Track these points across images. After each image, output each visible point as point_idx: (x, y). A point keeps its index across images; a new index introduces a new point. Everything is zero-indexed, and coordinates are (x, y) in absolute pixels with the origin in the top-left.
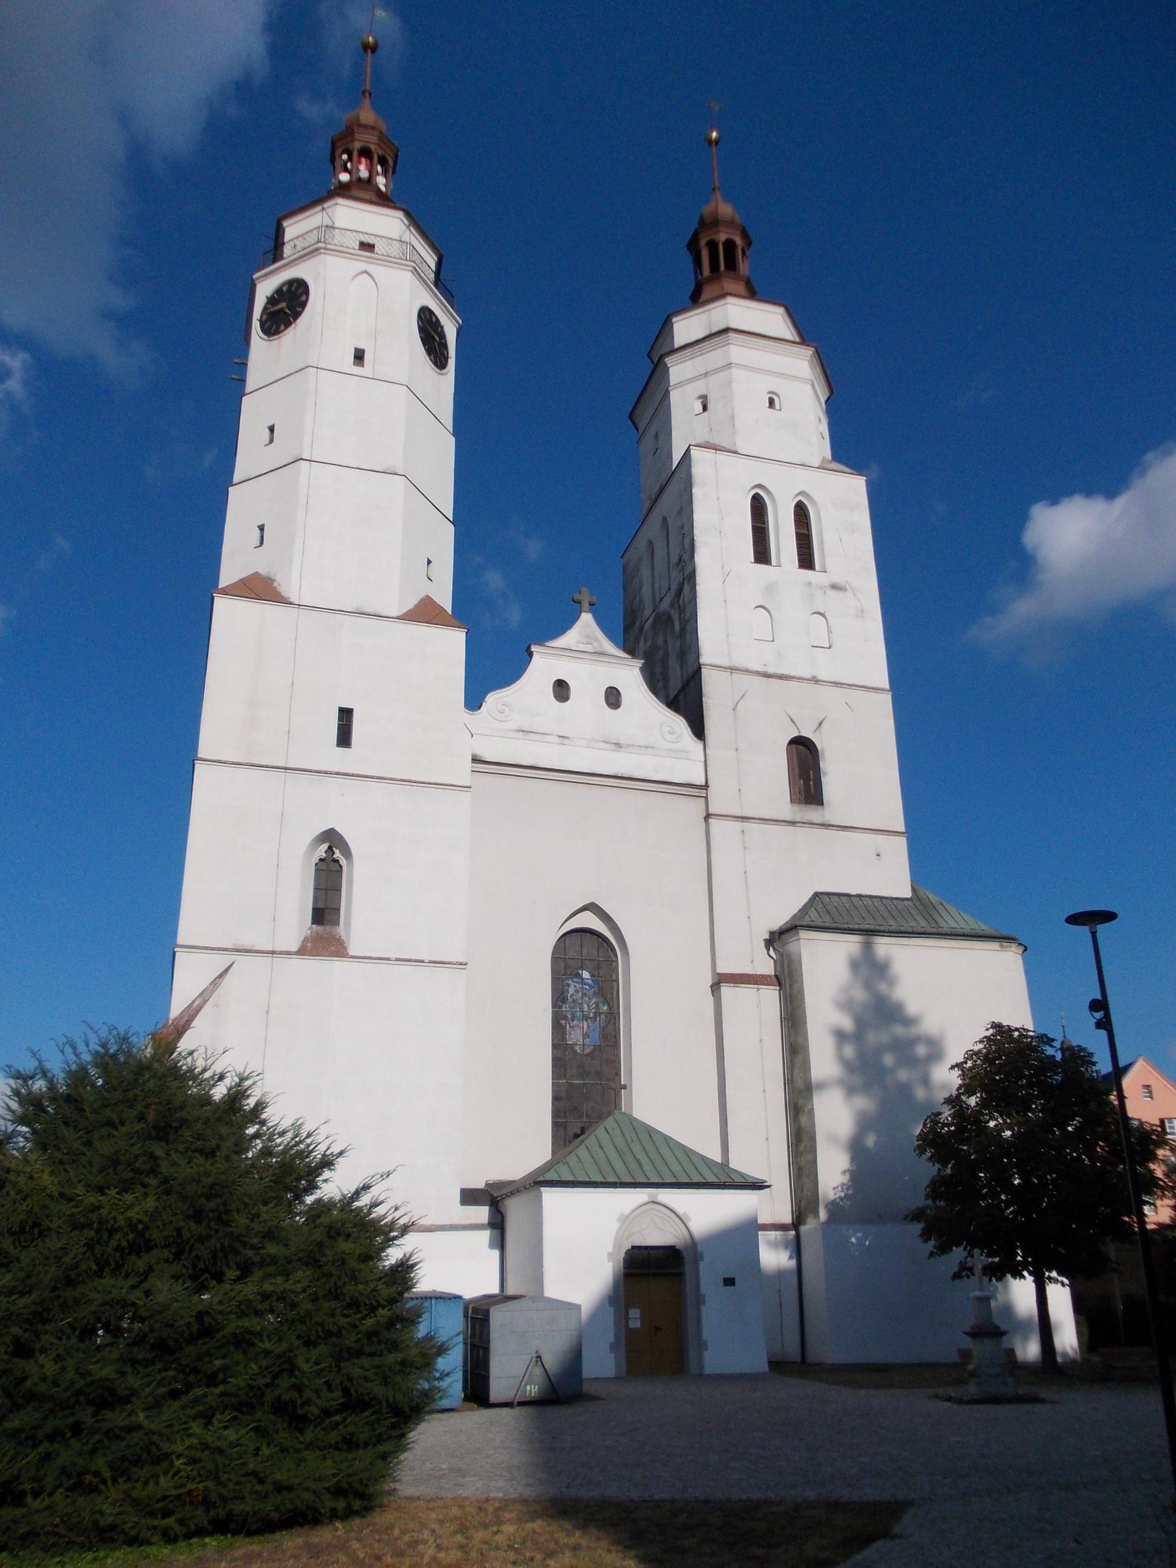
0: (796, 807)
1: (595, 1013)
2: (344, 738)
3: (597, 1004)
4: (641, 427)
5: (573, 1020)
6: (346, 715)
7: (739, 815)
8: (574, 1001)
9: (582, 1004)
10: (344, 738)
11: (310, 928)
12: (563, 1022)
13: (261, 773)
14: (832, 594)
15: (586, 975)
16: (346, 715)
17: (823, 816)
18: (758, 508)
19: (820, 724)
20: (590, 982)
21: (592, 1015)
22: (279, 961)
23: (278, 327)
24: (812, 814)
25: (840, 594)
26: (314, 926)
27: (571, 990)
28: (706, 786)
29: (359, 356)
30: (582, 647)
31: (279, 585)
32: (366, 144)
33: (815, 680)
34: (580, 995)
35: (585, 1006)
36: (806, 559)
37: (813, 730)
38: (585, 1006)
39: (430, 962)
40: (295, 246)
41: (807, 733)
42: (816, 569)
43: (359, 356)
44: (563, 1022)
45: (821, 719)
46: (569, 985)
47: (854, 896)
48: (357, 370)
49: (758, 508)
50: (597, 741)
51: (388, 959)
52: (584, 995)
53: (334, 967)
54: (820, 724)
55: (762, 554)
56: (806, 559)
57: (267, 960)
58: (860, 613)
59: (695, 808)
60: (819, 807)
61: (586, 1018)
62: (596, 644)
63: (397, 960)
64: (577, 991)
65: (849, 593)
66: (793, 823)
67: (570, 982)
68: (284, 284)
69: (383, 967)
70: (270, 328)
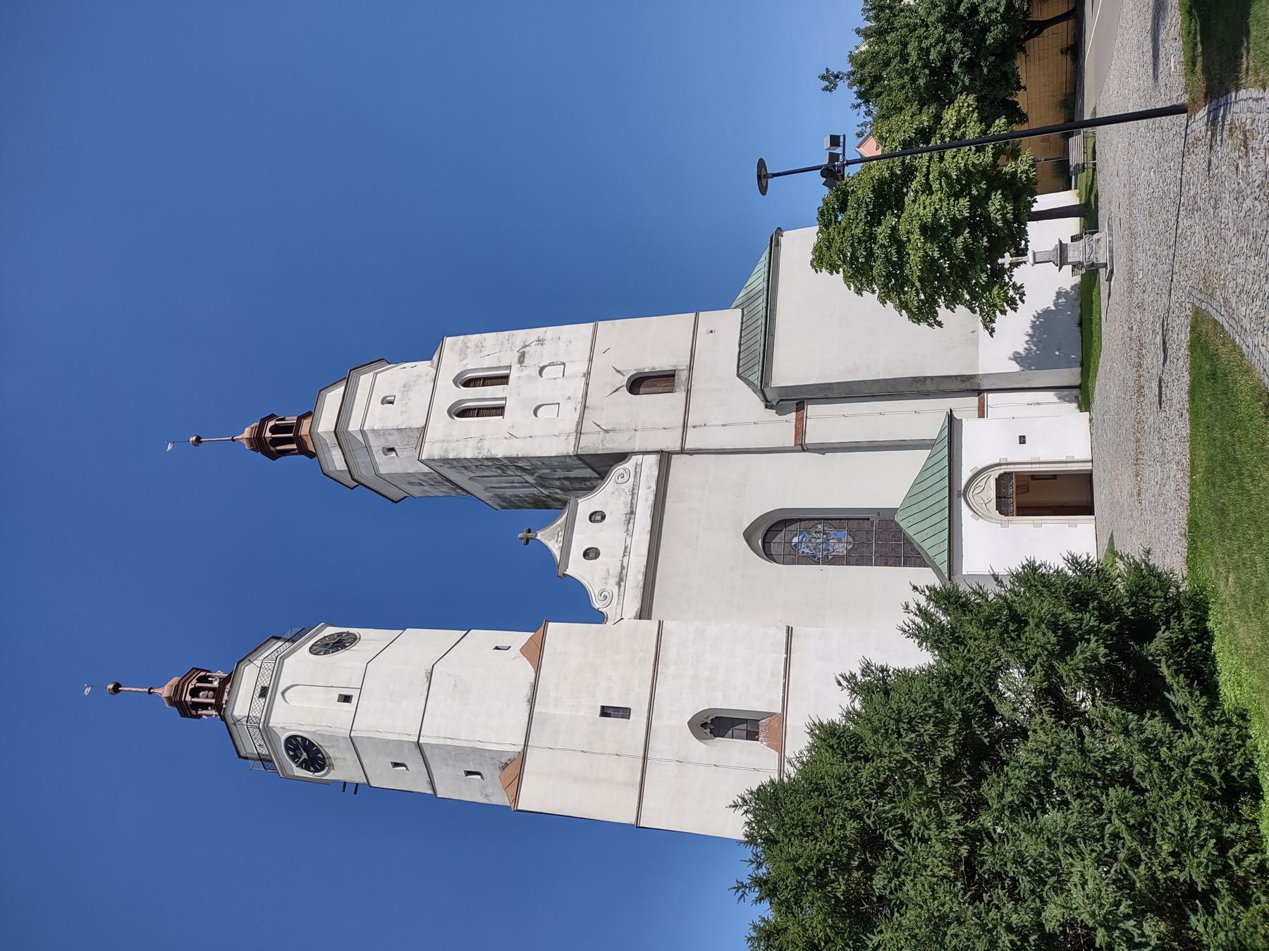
2: (624, 713)
5: (829, 550)
6: (606, 712)
10: (624, 713)
12: (830, 557)
15: (795, 540)
16: (606, 712)
19: (618, 371)
25: (527, 356)
27: (807, 550)
29: (347, 699)
33: (587, 375)
34: (810, 544)
35: (818, 541)
38: (818, 541)
40: (260, 745)
43: (347, 699)
44: (830, 557)
48: (354, 700)
49: (465, 413)
54: (618, 371)
55: (498, 411)
56: (503, 380)
64: (808, 547)
66: (688, 392)
70: (319, 765)
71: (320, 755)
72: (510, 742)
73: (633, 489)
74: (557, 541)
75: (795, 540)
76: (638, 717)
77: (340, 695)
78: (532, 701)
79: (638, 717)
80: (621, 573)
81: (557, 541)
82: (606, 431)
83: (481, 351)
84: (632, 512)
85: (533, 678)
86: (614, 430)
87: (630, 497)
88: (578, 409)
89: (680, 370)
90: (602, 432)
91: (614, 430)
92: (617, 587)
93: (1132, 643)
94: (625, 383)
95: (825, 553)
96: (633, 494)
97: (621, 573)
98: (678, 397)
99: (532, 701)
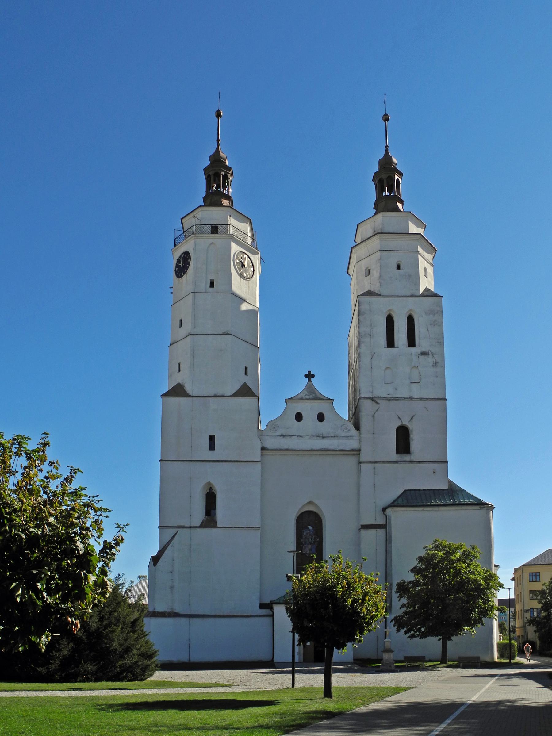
0: (399, 455)
1: (314, 542)
2: (212, 447)
3: (315, 538)
4: (351, 275)
5: (305, 544)
7: (373, 461)
8: (306, 538)
9: (308, 539)
10: (212, 447)
11: (205, 518)
12: (301, 546)
13: (182, 463)
14: (422, 358)
15: (310, 527)
17: (411, 458)
18: (390, 321)
19: (412, 418)
20: (312, 530)
21: (313, 542)
22: (194, 530)
23: (181, 274)
24: (407, 458)
25: (426, 357)
26: (206, 517)
27: (305, 534)
28: (360, 450)
29: (212, 284)
30: (308, 397)
31: (186, 388)
32: (216, 171)
33: (411, 398)
34: (308, 535)
35: (310, 539)
36: (411, 342)
37: (408, 421)
38: (310, 539)
39: (246, 527)
41: (406, 423)
42: (416, 346)
43: (212, 284)
44: (301, 546)
45: (412, 416)
46: (304, 532)
47: (422, 490)
48: (211, 290)
49: (390, 321)
50: (313, 436)
51: (231, 527)
52: (310, 535)
53: (214, 531)
54: (412, 418)
57: (188, 530)
58: (435, 365)
59: (351, 461)
60: (409, 455)
61: (310, 543)
62: (314, 395)
63: (235, 527)
64: (307, 534)
65: (430, 356)
66: (397, 462)
67: (304, 531)
68: (179, 261)
69: (230, 530)
71: (183, 274)
72: (385, 523)
73: (337, 436)
74: (306, 395)
75: (310, 527)
76: (210, 455)
77: (214, 280)
78: (216, 396)
79: (210, 455)
80: (288, 436)
81: (306, 395)
82: (373, 416)
83: (431, 325)
84: (323, 437)
85: (227, 395)
86: (374, 420)
87: (333, 435)
88: (388, 396)
89: (411, 456)
90: (372, 413)
91: (374, 420)
92: (280, 435)
93: (60, 557)
94: (404, 423)
95: (304, 543)
96: (335, 437)
97: (288, 436)
98: (394, 456)
99: (216, 396)
